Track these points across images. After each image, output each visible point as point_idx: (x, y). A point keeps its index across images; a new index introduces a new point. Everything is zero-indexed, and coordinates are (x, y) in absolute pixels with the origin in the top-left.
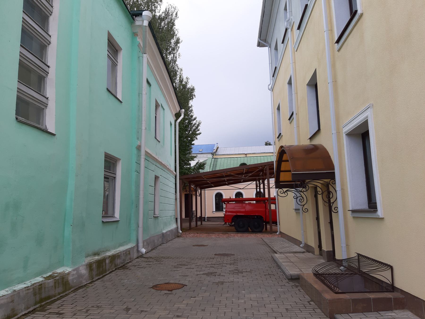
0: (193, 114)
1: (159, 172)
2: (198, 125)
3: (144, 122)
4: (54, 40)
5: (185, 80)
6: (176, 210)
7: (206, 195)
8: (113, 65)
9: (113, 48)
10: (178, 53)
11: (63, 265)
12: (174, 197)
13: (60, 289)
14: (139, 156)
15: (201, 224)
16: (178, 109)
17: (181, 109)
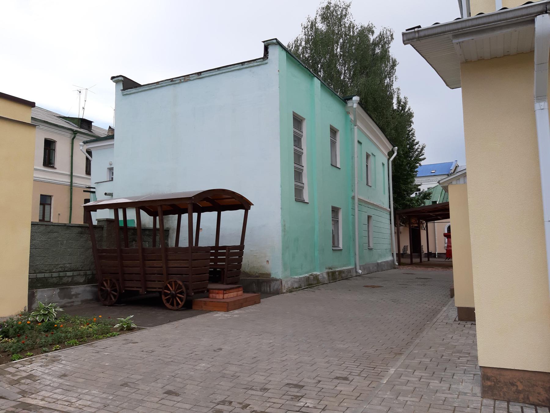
0: (414, 138)
1: (371, 212)
2: (422, 149)
3: (356, 179)
4: (305, 151)
5: (403, 100)
6: (391, 244)
7: (436, 228)
8: (333, 143)
9: (334, 132)
10: (394, 76)
11: (315, 271)
12: (389, 232)
13: (315, 282)
14: (354, 204)
15: (429, 260)
16: (390, 147)
17: (394, 147)
